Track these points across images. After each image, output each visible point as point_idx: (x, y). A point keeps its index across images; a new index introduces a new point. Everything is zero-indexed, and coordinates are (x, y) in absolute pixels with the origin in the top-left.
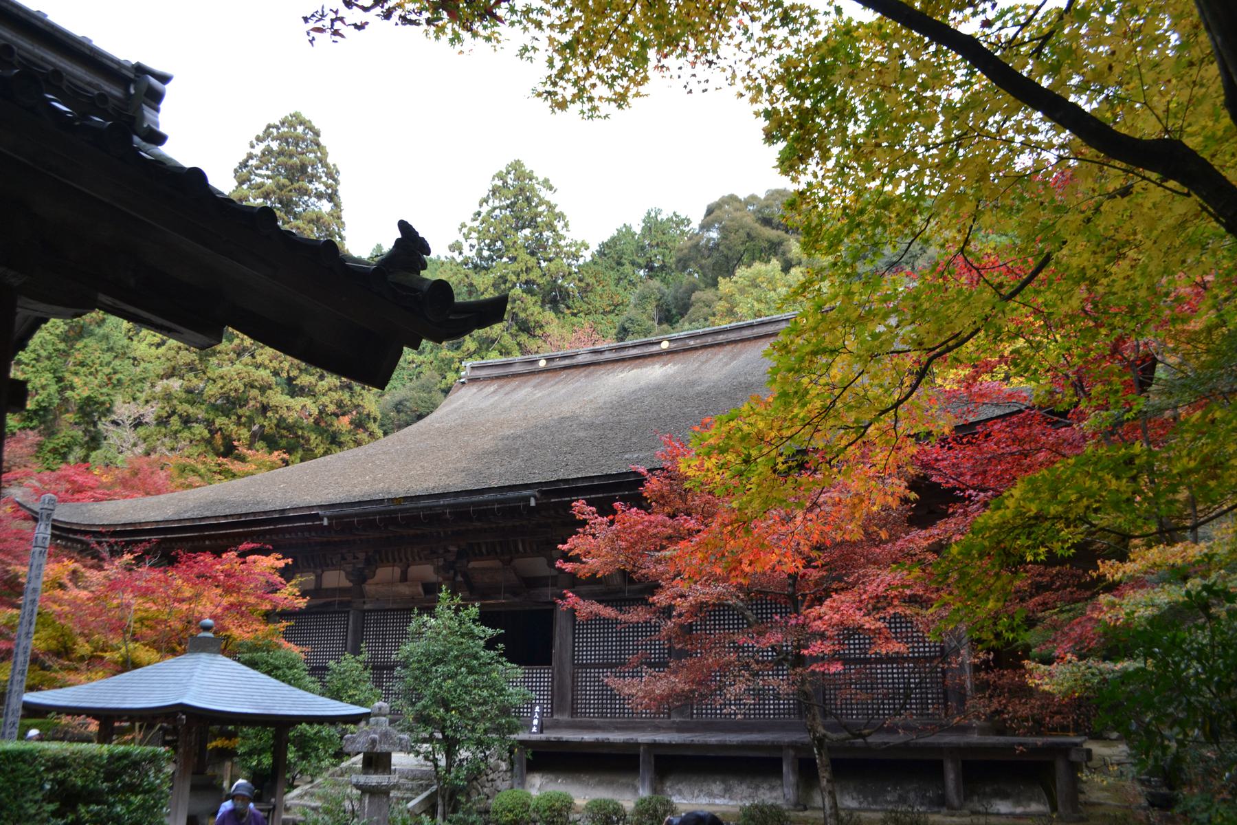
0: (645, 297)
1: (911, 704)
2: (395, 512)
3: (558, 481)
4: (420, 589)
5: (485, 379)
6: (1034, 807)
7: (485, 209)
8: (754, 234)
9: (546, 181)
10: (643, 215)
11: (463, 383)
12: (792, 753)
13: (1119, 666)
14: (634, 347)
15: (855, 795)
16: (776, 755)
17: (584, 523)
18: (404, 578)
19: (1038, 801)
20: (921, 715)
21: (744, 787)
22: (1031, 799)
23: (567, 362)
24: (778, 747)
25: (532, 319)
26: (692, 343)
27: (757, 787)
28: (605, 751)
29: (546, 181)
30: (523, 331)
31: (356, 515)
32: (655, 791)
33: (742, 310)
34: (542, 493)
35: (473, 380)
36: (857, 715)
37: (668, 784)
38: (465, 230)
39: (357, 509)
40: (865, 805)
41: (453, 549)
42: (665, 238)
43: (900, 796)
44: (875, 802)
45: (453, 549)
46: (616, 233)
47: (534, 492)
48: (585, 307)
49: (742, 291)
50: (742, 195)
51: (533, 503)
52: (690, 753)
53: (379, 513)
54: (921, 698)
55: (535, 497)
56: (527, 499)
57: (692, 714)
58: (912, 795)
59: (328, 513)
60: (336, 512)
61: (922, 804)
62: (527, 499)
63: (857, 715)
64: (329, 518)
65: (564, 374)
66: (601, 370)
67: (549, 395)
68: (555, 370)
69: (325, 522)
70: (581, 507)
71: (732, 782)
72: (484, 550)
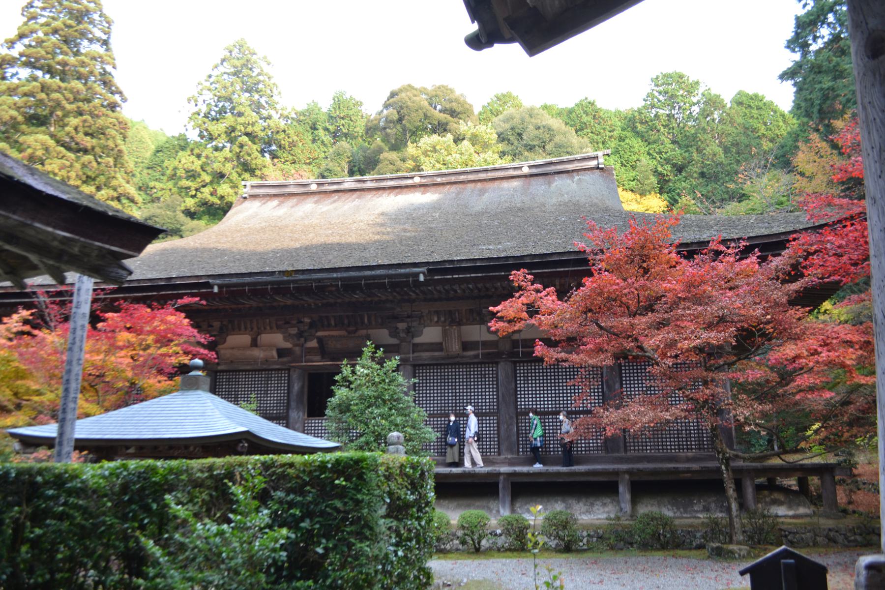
0: (339, 154)
1: (691, 441)
2: (289, 282)
3: (444, 261)
4: (275, 353)
5: (264, 196)
6: (802, 510)
7: (215, 73)
8: (429, 115)
9: (265, 58)
10: (333, 95)
11: (245, 198)
12: (627, 477)
13: (143, 462)
14: (391, 179)
15: (670, 507)
16: (613, 478)
17: (520, 288)
18: (254, 344)
19: (804, 506)
20: (700, 449)
21: (581, 504)
22: (799, 505)
23: (335, 187)
24: (616, 473)
25: (254, 162)
26: (439, 180)
27: (592, 505)
28: (469, 480)
29: (265, 58)
30: (246, 171)
31: (248, 284)
32: (513, 511)
33: (428, 170)
34: (429, 270)
35: (254, 196)
36: (651, 450)
37: (518, 505)
38: (200, 87)
39: (247, 280)
40: (678, 514)
41: (307, 320)
42: (351, 113)
43: (704, 507)
44: (686, 512)
45: (307, 320)
46: (325, 105)
47: (424, 269)
48: (291, 157)
49: (425, 154)
50: (417, 86)
51: (422, 278)
52: (542, 480)
53: (272, 283)
54: (699, 437)
55: (424, 273)
56: (417, 275)
57: (519, 451)
58: (713, 505)
59: (219, 281)
60: (226, 281)
61: (721, 512)
62: (417, 275)
63: (651, 450)
64: (220, 286)
65: (336, 196)
66: (369, 196)
67: (335, 209)
68: (325, 192)
69: (216, 289)
70: (519, 276)
71: (591, 500)
72: (333, 323)
